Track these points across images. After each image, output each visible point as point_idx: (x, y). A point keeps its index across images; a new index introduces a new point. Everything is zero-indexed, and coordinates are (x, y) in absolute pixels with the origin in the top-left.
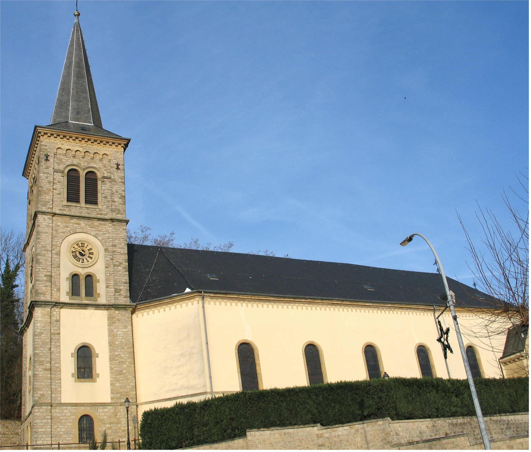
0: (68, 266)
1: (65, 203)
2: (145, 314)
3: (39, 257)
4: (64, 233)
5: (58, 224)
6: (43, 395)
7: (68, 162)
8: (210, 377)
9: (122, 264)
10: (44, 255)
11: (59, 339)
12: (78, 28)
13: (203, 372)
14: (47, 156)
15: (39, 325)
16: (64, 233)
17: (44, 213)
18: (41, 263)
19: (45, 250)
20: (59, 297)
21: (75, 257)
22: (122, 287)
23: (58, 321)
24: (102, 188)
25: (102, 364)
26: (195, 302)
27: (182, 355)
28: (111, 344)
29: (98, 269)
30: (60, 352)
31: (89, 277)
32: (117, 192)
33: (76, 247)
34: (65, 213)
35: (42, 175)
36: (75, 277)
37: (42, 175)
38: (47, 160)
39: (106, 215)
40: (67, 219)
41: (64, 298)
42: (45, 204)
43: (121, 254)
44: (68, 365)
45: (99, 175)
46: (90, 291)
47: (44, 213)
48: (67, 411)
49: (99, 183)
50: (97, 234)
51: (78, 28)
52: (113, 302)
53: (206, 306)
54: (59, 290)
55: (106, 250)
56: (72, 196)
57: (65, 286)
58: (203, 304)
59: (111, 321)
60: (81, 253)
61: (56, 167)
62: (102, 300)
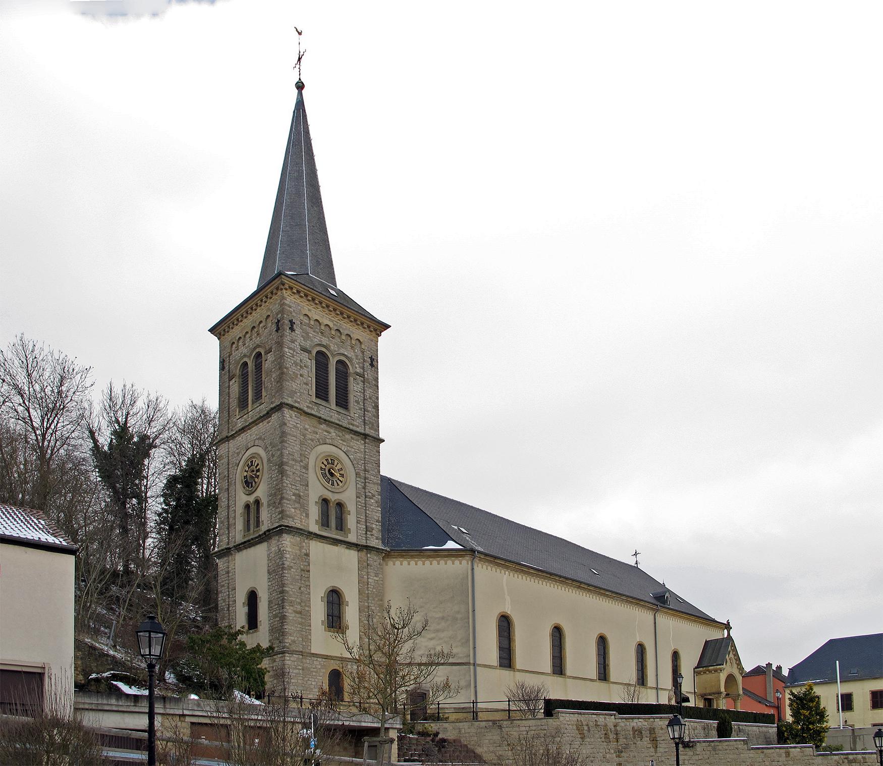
0: (316, 489)
1: (314, 399)
2: (398, 563)
3: (286, 468)
4: (312, 440)
5: (307, 426)
6: (294, 642)
7: (317, 339)
8: (475, 648)
9: (374, 496)
10: (292, 466)
11: (309, 577)
12: (300, 105)
13: (468, 640)
14: (292, 323)
15: (288, 556)
16: (312, 440)
17: (291, 407)
18: (287, 476)
19: (293, 460)
20: (308, 524)
21: (324, 475)
22: (374, 526)
23: (307, 555)
24: (355, 388)
25: (351, 614)
26: (464, 562)
27: (443, 618)
28: (360, 592)
29: (348, 496)
30: (309, 594)
31: (340, 505)
32: (370, 398)
33: (326, 463)
34: (313, 412)
35: (287, 350)
36: (247, 506)
37: (287, 350)
38: (292, 329)
39: (358, 427)
40: (314, 421)
41: (314, 528)
42: (292, 394)
43: (374, 484)
44: (318, 611)
45: (351, 370)
46: (341, 526)
47: (291, 407)
48: (318, 662)
49: (351, 379)
50: (348, 451)
51: (300, 105)
52: (363, 542)
53: (475, 567)
54: (307, 516)
55: (357, 474)
56: (322, 392)
57: (314, 512)
58: (472, 565)
59: (363, 566)
60: (330, 473)
61: (308, 345)
62: (352, 538)
